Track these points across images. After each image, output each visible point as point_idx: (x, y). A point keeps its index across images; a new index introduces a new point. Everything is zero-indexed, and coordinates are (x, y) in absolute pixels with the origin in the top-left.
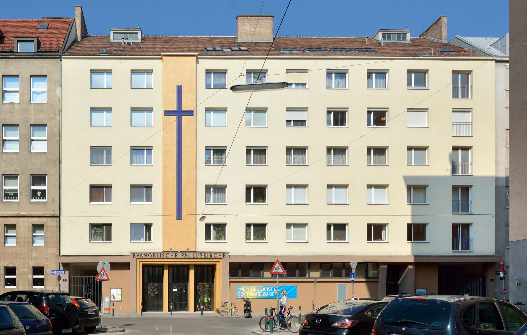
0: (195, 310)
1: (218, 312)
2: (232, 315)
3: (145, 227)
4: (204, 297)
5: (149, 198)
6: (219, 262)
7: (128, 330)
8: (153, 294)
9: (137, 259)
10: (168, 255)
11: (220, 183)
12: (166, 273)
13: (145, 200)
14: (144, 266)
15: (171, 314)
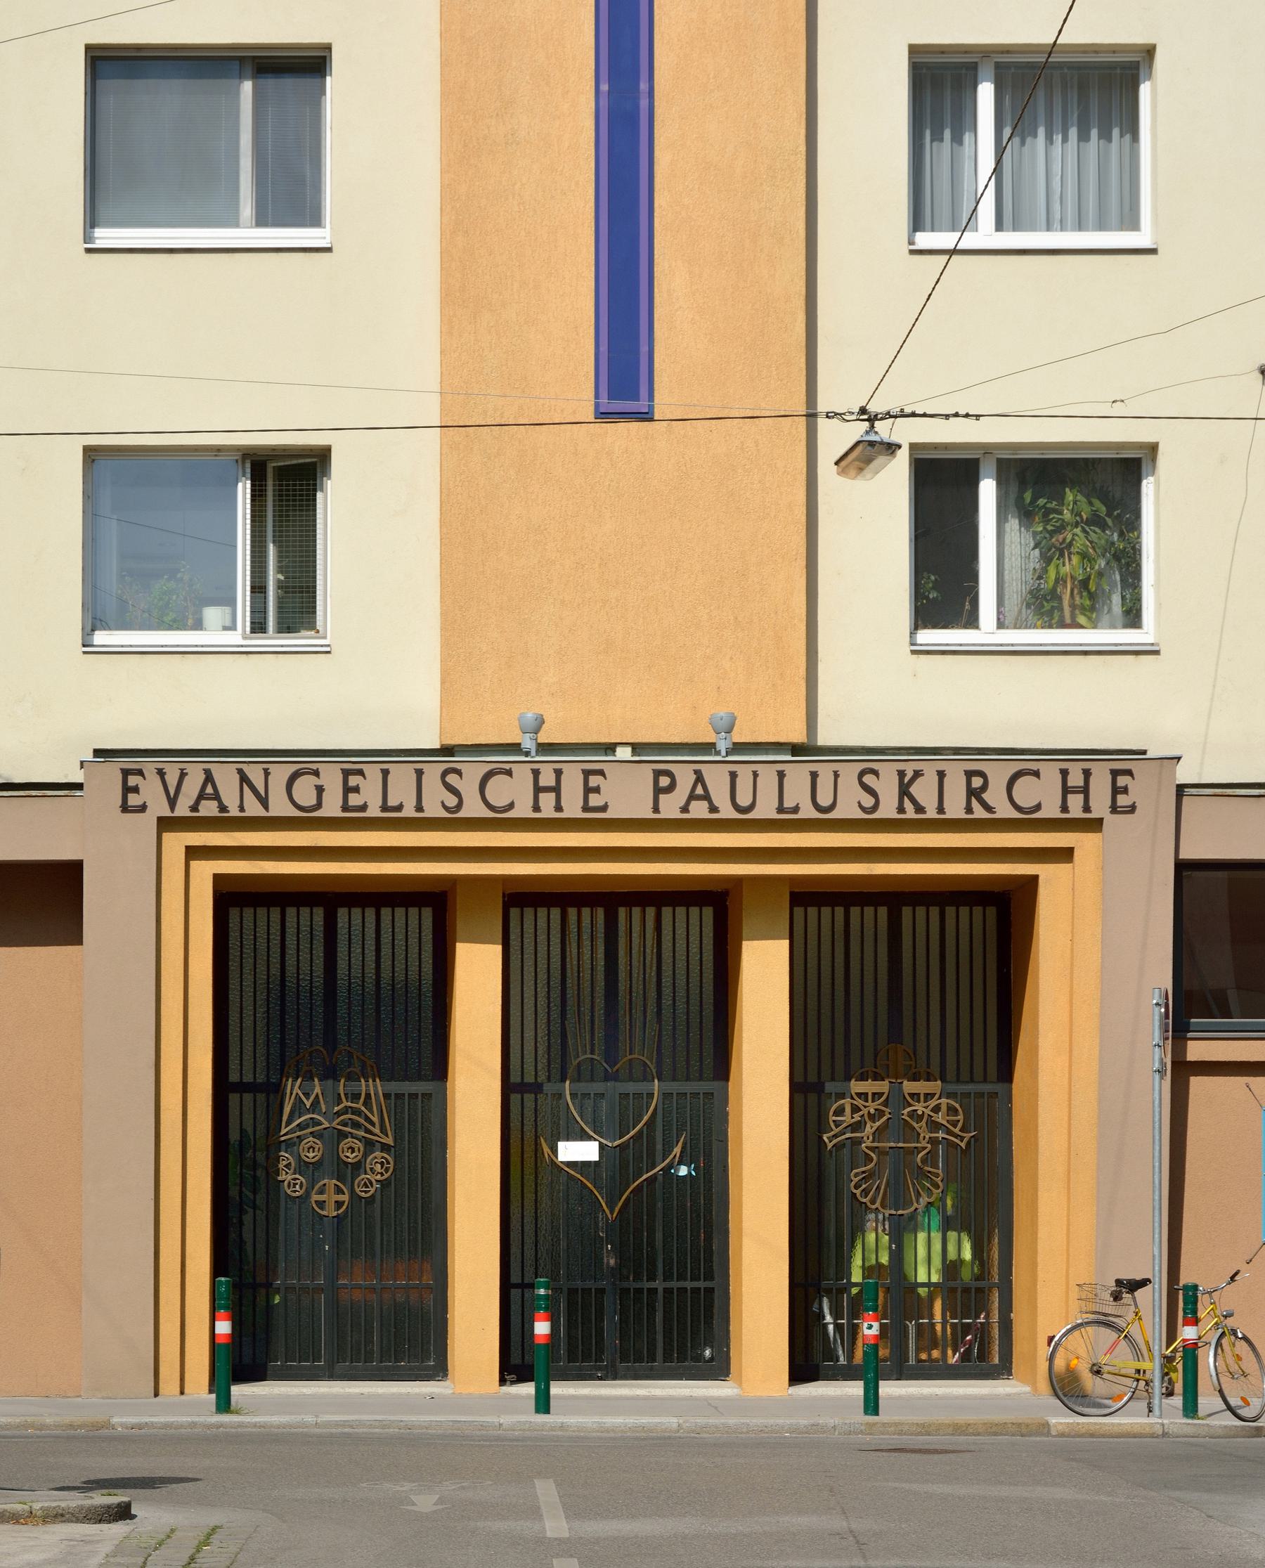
0: (806, 1364)
1: (1067, 1389)
2: (1191, 1408)
3: (244, 490)
4: (900, 1231)
5: (291, 192)
6: (1065, 855)
7: (152, 1515)
8: (330, 1199)
9: (165, 824)
10: (499, 791)
11: (1095, 28)
12: (478, 971)
13: (247, 209)
14: (231, 898)
15: (543, 1403)
